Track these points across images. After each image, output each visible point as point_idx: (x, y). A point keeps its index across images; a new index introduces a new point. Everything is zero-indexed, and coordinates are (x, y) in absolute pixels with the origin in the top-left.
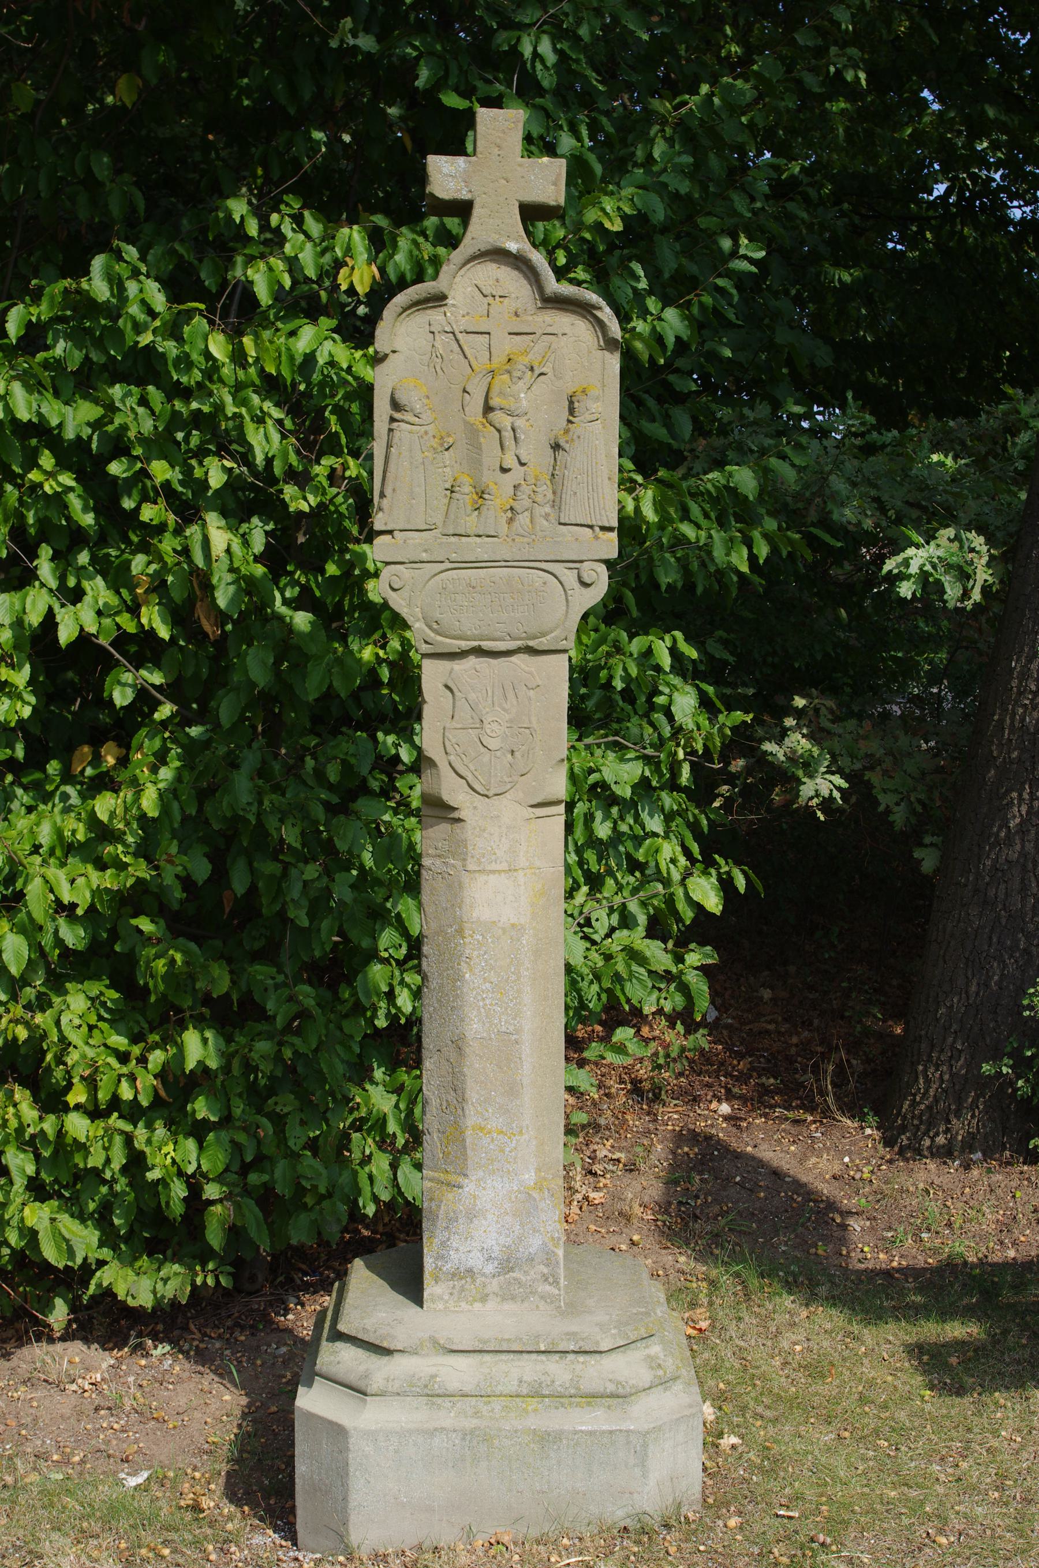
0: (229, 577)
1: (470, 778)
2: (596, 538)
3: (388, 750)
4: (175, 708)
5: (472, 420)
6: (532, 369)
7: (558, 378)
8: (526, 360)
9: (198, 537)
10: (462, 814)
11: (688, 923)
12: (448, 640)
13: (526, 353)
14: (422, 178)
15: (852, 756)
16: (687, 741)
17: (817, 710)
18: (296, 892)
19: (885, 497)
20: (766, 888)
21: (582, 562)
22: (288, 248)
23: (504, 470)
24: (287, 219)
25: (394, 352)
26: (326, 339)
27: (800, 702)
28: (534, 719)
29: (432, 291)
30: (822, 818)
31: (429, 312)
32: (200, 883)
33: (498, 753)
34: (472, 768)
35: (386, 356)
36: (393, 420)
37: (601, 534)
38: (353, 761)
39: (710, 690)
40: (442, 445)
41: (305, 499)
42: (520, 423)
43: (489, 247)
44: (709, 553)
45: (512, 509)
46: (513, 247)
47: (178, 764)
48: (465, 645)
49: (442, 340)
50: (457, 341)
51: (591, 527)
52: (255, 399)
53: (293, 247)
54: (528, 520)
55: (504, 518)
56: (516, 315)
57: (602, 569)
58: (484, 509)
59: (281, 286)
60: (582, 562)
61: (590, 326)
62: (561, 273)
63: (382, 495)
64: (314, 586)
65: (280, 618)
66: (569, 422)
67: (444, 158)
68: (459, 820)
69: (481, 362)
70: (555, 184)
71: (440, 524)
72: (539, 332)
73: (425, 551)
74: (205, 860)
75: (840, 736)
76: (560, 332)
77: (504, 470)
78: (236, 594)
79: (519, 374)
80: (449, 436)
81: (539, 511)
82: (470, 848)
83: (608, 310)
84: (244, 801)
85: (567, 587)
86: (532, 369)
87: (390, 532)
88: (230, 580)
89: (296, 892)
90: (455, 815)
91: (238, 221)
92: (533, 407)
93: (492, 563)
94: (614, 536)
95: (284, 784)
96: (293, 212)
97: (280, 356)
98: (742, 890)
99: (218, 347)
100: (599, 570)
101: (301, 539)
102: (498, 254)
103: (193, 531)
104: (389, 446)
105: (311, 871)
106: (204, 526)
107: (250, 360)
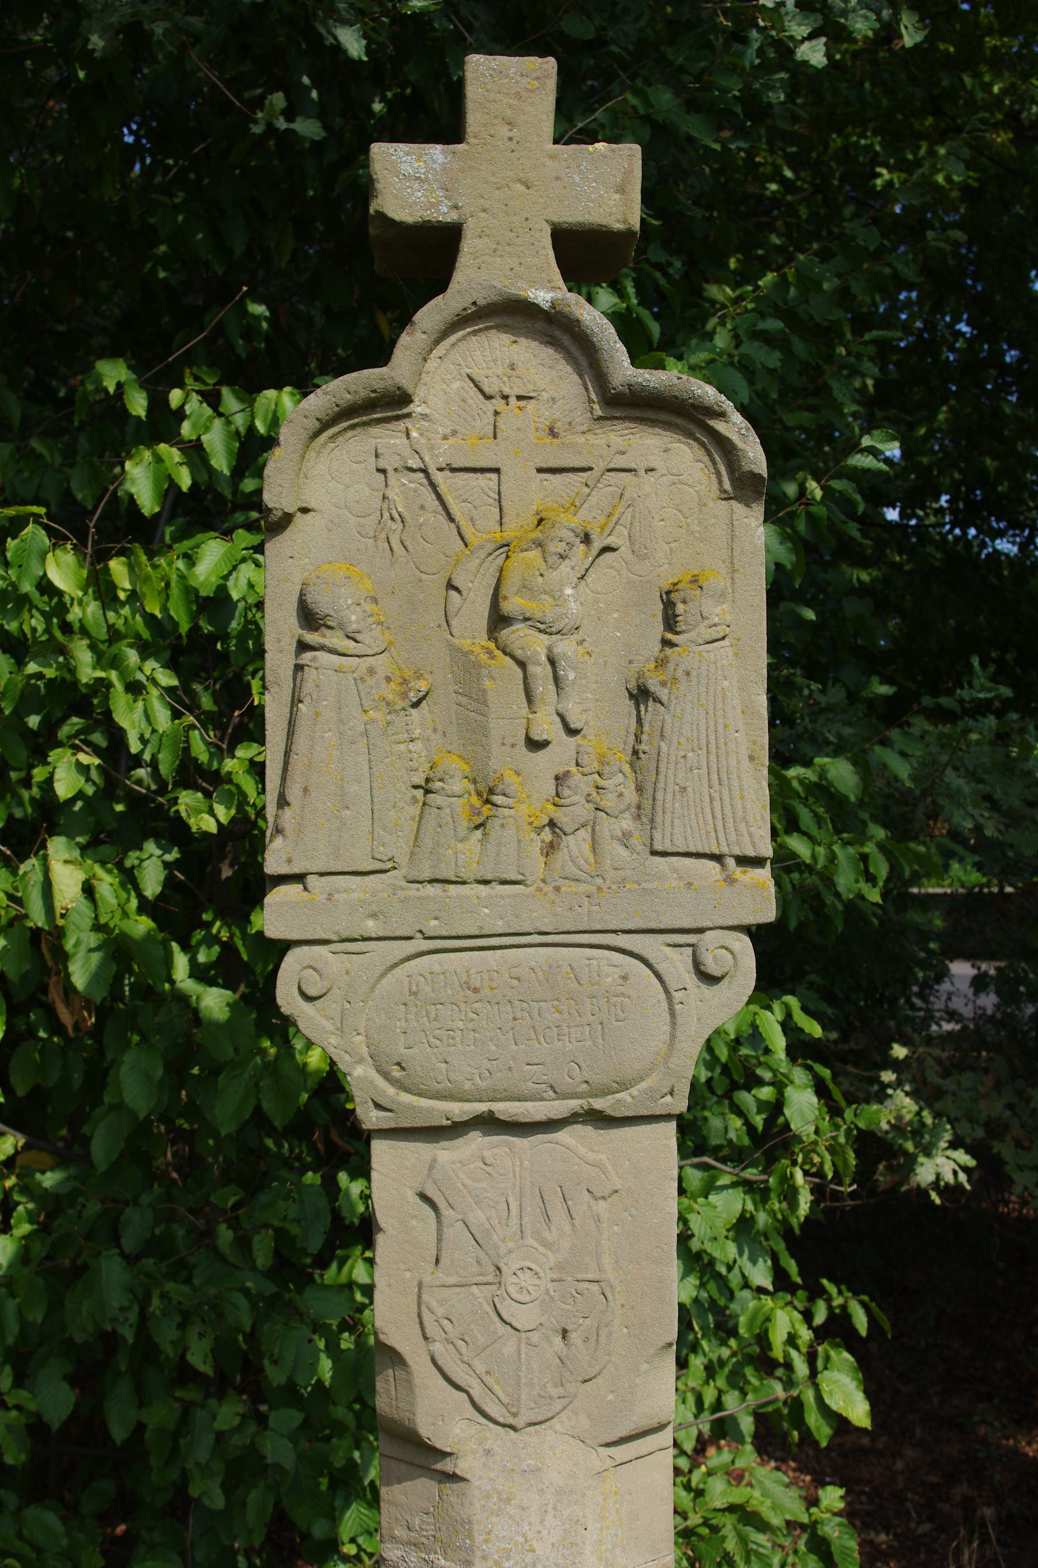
0: (93, 939)
1: (477, 1391)
2: (730, 880)
3: (352, 1207)
4: (21, 1142)
5: (466, 644)
6: (587, 539)
7: (640, 555)
8: (575, 522)
9: (38, 877)
10: (462, 1467)
11: (824, 1444)
12: (424, 1102)
13: (574, 507)
14: (364, 189)
15: (972, 1120)
16: (807, 1160)
17: (921, 1061)
18: (202, 1451)
19: (998, 795)
20: (893, 1326)
21: (701, 931)
22: (186, 429)
23: (535, 745)
24: (195, 397)
25: (305, 510)
26: (244, 560)
27: (900, 1052)
28: (607, 1262)
29: (379, 386)
30: (938, 1201)
31: (375, 430)
32: (55, 1426)
33: (535, 1337)
34: (481, 1369)
35: (287, 520)
36: (303, 647)
37: (738, 872)
38: (295, 1230)
39: (826, 1073)
40: (404, 695)
41: (211, 812)
42: (565, 647)
43: (494, 298)
44: (829, 881)
45: (552, 824)
46: (542, 297)
47: (26, 1228)
48: (461, 1110)
49: (405, 490)
50: (433, 485)
51: (718, 858)
52: (132, 656)
53: (194, 426)
54: (586, 848)
55: (536, 843)
56: (552, 433)
57: (744, 945)
58: (494, 826)
59: (173, 485)
60: (701, 931)
61: (701, 453)
62: (642, 350)
63: (283, 802)
64: (239, 943)
65: (182, 998)
66: (666, 643)
67: (403, 147)
68: (454, 1478)
69: (483, 529)
70: (621, 190)
71: (402, 859)
72: (600, 466)
73: (374, 916)
74: (65, 1386)
75: (954, 1094)
76: (641, 467)
77: (535, 745)
78: (102, 966)
79: (561, 548)
80: (419, 676)
81: (608, 827)
82: (479, 1539)
83: (737, 418)
84: (116, 1304)
85: (672, 986)
86: (587, 539)
87: (299, 878)
88: (93, 945)
89: (202, 1451)
90: (447, 1466)
91: (112, 390)
92: (594, 618)
93: (514, 938)
94: (764, 875)
95: (192, 1260)
96: (203, 388)
97: (168, 585)
98: (863, 1331)
99: (63, 570)
100: (736, 947)
101: (226, 872)
102: (512, 313)
103: (30, 866)
104: (296, 700)
105: (228, 1413)
106: (45, 859)
107: (122, 596)
